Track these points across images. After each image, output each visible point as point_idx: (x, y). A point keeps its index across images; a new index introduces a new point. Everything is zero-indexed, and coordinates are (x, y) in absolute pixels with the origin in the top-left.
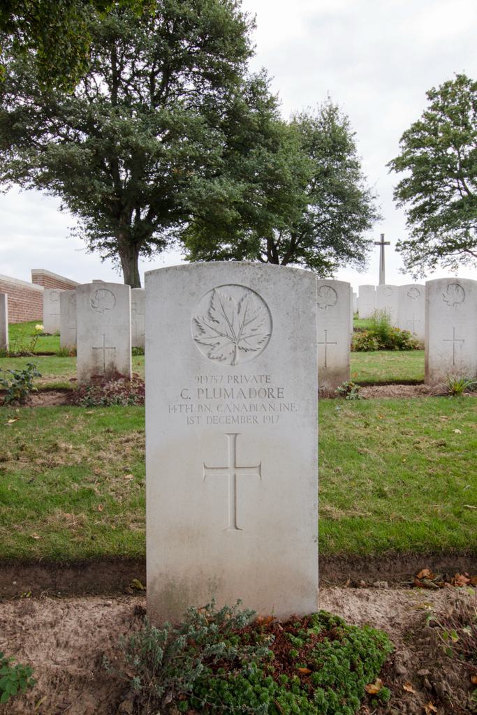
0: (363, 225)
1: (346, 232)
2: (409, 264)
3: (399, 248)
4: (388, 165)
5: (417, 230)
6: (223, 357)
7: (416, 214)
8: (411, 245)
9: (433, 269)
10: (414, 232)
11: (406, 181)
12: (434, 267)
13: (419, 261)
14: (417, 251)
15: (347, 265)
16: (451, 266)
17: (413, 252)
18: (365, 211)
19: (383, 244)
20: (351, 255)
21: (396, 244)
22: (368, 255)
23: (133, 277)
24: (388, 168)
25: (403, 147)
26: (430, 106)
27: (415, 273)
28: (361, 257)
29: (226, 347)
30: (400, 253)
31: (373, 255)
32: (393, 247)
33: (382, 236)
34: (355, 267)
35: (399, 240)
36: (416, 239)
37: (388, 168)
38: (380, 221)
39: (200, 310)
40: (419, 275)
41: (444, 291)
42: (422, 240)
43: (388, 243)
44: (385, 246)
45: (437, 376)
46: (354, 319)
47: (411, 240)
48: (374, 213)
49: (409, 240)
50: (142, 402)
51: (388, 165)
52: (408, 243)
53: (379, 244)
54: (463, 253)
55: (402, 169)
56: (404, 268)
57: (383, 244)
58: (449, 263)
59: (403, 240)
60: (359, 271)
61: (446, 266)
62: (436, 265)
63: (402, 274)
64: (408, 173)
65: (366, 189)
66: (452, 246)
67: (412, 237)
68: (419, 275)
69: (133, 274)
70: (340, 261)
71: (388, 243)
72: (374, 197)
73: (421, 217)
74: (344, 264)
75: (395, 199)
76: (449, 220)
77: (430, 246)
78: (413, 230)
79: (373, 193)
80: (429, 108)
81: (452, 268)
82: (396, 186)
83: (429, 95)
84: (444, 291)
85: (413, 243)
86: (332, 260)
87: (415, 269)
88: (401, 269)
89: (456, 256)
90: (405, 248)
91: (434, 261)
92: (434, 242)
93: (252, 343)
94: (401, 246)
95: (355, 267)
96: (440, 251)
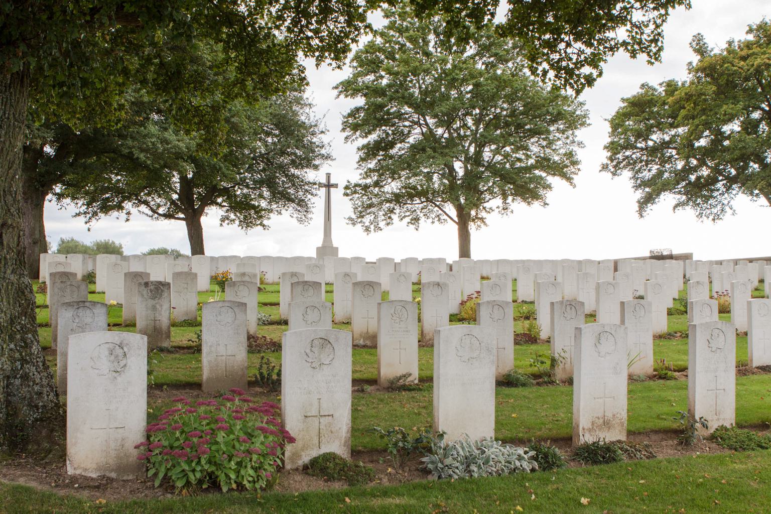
0: (307, 162)
1: (282, 168)
2: (361, 212)
3: (348, 191)
4: (336, 88)
5: (370, 170)
6: (199, 332)
7: (370, 151)
8: (362, 189)
9: (389, 221)
10: (366, 173)
11: (358, 110)
12: (390, 218)
13: (372, 209)
14: (370, 196)
15: (283, 211)
16: (411, 217)
17: (365, 198)
18: (310, 149)
19: (329, 186)
20: (289, 199)
21: (344, 186)
22: (312, 201)
23: (38, 229)
24: (336, 92)
25: (354, 67)
26: (386, 25)
27: (367, 224)
28: (301, 203)
29: (398, 320)
30: (350, 197)
31: (317, 202)
32: (340, 190)
33: (328, 176)
34: (295, 216)
35: (349, 182)
36: (369, 181)
37: (336, 92)
38: (329, 162)
39: (392, 311)
40: (372, 227)
41: (431, 288)
42: (377, 184)
43: (336, 186)
44: (332, 190)
45: (428, 338)
46: (327, 292)
47: (363, 182)
48: (323, 151)
49: (360, 182)
50: (66, 395)
51: (336, 88)
52: (360, 185)
53: (325, 186)
54: (425, 204)
55: (353, 95)
56: (354, 216)
57: (329, 186)
58: (408, 214)
59: (353, 182)
60: (300, 221)
61: (405, 216)
62: (393, 216)
63: (351, 226)
64: (360, 101)
65: (312, 120)
66: (412, 193)
67: (364, 178)
68: (372, 227)
69: (37, 225)
70: (274, 206)
71: (336, 186)
72: (322, 132)
73: (375, 155)
74: (279, 209)
75: (344, 130)
76: (410, 162)
77: (386, 190)
78: (365, 170)
79: (321, 127)
80: (385, 27)
81: (412, 220)
82: (345, 114)
83: (385, 13)
84: (431, 288)
85: (366, 187)
86: (263, 204)
87: (367, 219)
88: (350, 219)
89: (417, 205)
90: (355, 192)
91: (392, 211)
92: (392, 186)
93: (403, 319)
94: (350, 190)
95: (295, 216)
96: (397, 198)
